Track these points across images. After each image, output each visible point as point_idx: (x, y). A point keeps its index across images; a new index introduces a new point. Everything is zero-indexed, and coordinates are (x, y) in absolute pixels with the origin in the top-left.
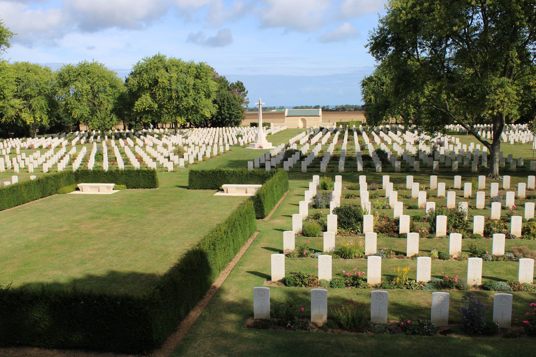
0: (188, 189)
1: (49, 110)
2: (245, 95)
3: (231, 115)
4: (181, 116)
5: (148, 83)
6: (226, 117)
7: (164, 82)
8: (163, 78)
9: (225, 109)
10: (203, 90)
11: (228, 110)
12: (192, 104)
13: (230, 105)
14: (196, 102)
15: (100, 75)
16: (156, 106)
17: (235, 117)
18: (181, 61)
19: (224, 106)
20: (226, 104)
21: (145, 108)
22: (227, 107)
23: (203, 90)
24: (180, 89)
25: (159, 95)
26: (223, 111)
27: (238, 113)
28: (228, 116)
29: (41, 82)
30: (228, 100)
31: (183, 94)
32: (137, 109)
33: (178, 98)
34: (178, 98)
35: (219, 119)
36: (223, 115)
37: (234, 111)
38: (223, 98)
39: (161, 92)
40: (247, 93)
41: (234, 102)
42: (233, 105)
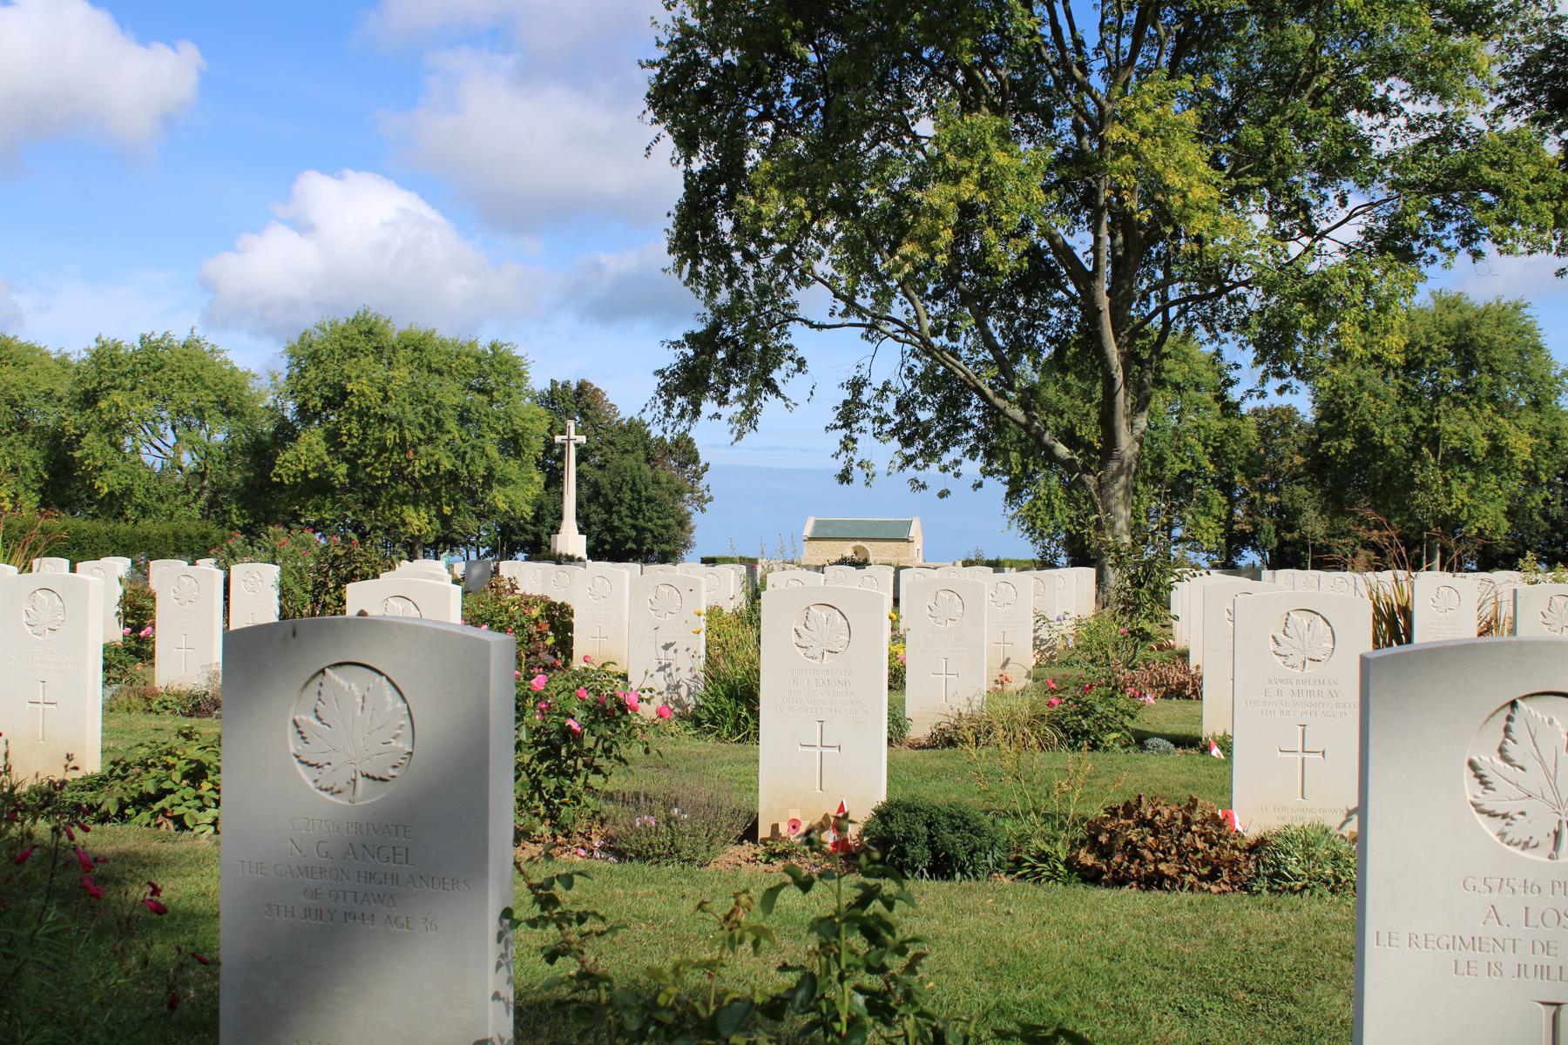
0: (770, 890)
1: (46, 476)
2: (698, 476)
3: (641, 530)
4: (416, 505)
5: (322, 396)
6: (627, 539)
7: (363, 394)
8: (363, 382)
9: (624, 511)
10: (493, 429)
11: (634, 517)
12: (447, 464)
13: (639, 501)
14: (463, 460)
15: (189, 373)
16: (343, 469)
17: (657, 539)
18: (437, 335)
19: (621, 501)
20: (627, 496)
21: (305, 473)
22: (630, 508)
23: (493, 429)
24: (411, 416)
25: (350, 436)
26: (615, 517)
27: (664, 527)
28: (634, 533)
29: (26, 392)
30: (634, 484)
31: (418, 433)
32: (280, 476)
33: (402, 445)
34: (402, 445)
35: (605, 542)
36: (618, 529)
37: (651, 520)
38: (618, 479)
39: (354, 425)
40: (705, 469)
41: (652, 492)
42: (649, 500)
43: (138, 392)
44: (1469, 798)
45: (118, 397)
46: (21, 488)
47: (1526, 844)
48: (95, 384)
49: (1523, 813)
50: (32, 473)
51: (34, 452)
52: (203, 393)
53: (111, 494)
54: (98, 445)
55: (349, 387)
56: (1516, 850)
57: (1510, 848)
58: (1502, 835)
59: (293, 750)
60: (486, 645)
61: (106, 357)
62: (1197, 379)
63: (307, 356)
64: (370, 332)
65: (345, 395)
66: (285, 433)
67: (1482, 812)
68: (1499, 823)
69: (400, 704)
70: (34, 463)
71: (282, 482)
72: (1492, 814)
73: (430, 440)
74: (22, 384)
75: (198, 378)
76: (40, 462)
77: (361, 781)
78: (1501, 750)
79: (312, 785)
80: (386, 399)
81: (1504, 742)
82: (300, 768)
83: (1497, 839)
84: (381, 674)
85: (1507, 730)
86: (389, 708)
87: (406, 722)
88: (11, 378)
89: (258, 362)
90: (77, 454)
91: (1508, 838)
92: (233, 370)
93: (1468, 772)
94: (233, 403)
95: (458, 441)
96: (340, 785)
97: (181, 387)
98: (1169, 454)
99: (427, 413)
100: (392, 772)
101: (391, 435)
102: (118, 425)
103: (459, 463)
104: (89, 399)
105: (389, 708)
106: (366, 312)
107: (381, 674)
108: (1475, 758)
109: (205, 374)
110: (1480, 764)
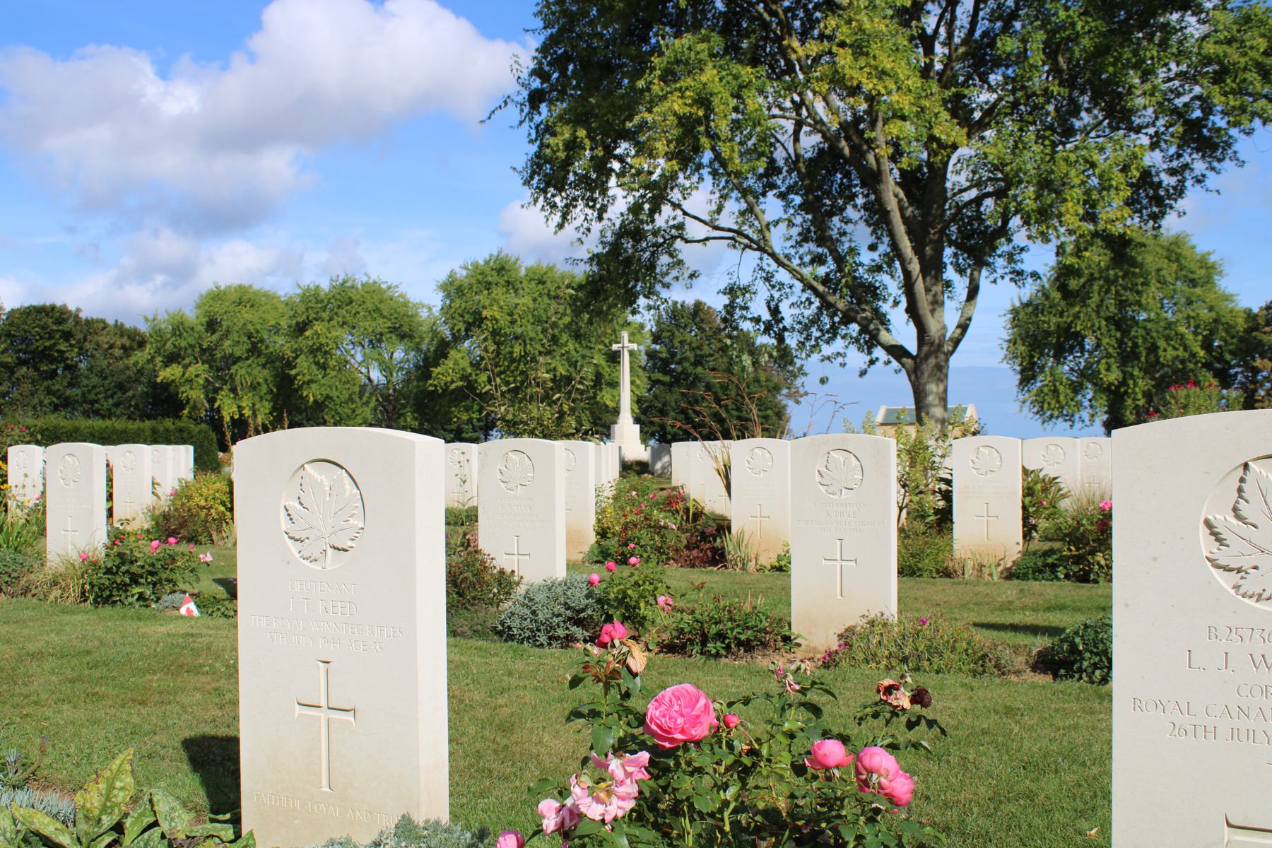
24: (532, 334)
29: (258, 327)
43: (334, 323)
44: (1205, 553)
45: (318, 327)
46: (257, 399)
47: (1260, 595)
48: (304, 317)
49: (1256, 568)
50: (264, 389)
51: (266, 372)
52: (381, 321)
53: (315, 401)
54: (306, 364)
55: (485, 313)
56: (1251, 602)
57: (1246, 600)
58: (1237, 587)
59: (284, 529)
60: (413, 442)
61: (312, 298)
62: (1191, 276)
63: (453, 289)
64: (503, 268)
65: (482, 320)
66: (443, 350)
67: (1218, 567)
68: (1234, 577)
69: (355, 490)
70: (266, 380)
71: (436, 390)
72: (1227, 569)
73: (549, 353)
74: (256, 320)
75: (377, 310)
76: (270, 379)
77: (330, 551)
78: (1235, 509)
79: (298, 556)
80: (513, 322)
81: (1237, 502)
82: (289, 542)
83: (1233, 592)
84: (342, 468)
85: (1240, 490)
86: (348, 494)
87: (359, 504)
88: (249, 317)
89: (423, 293)
90: (293, 372)
91: (1242, 591)
92: (406, 304)
93: (1203, 531)
94: (406, 329)
95: (573, 353)
96: (316, 555)
97: (365, 317)
98: (1162, 343)
99: (544, 331)
100: (350, 543)
101: (518, 350)
102: (319, 349)
103: (572, 370)
104: (300, 329)
105: (348, 494)
106: (499, 253)
107: (342, 468)
108: (1210, 517)
109: (382, 306)
110: (1214, 523)
